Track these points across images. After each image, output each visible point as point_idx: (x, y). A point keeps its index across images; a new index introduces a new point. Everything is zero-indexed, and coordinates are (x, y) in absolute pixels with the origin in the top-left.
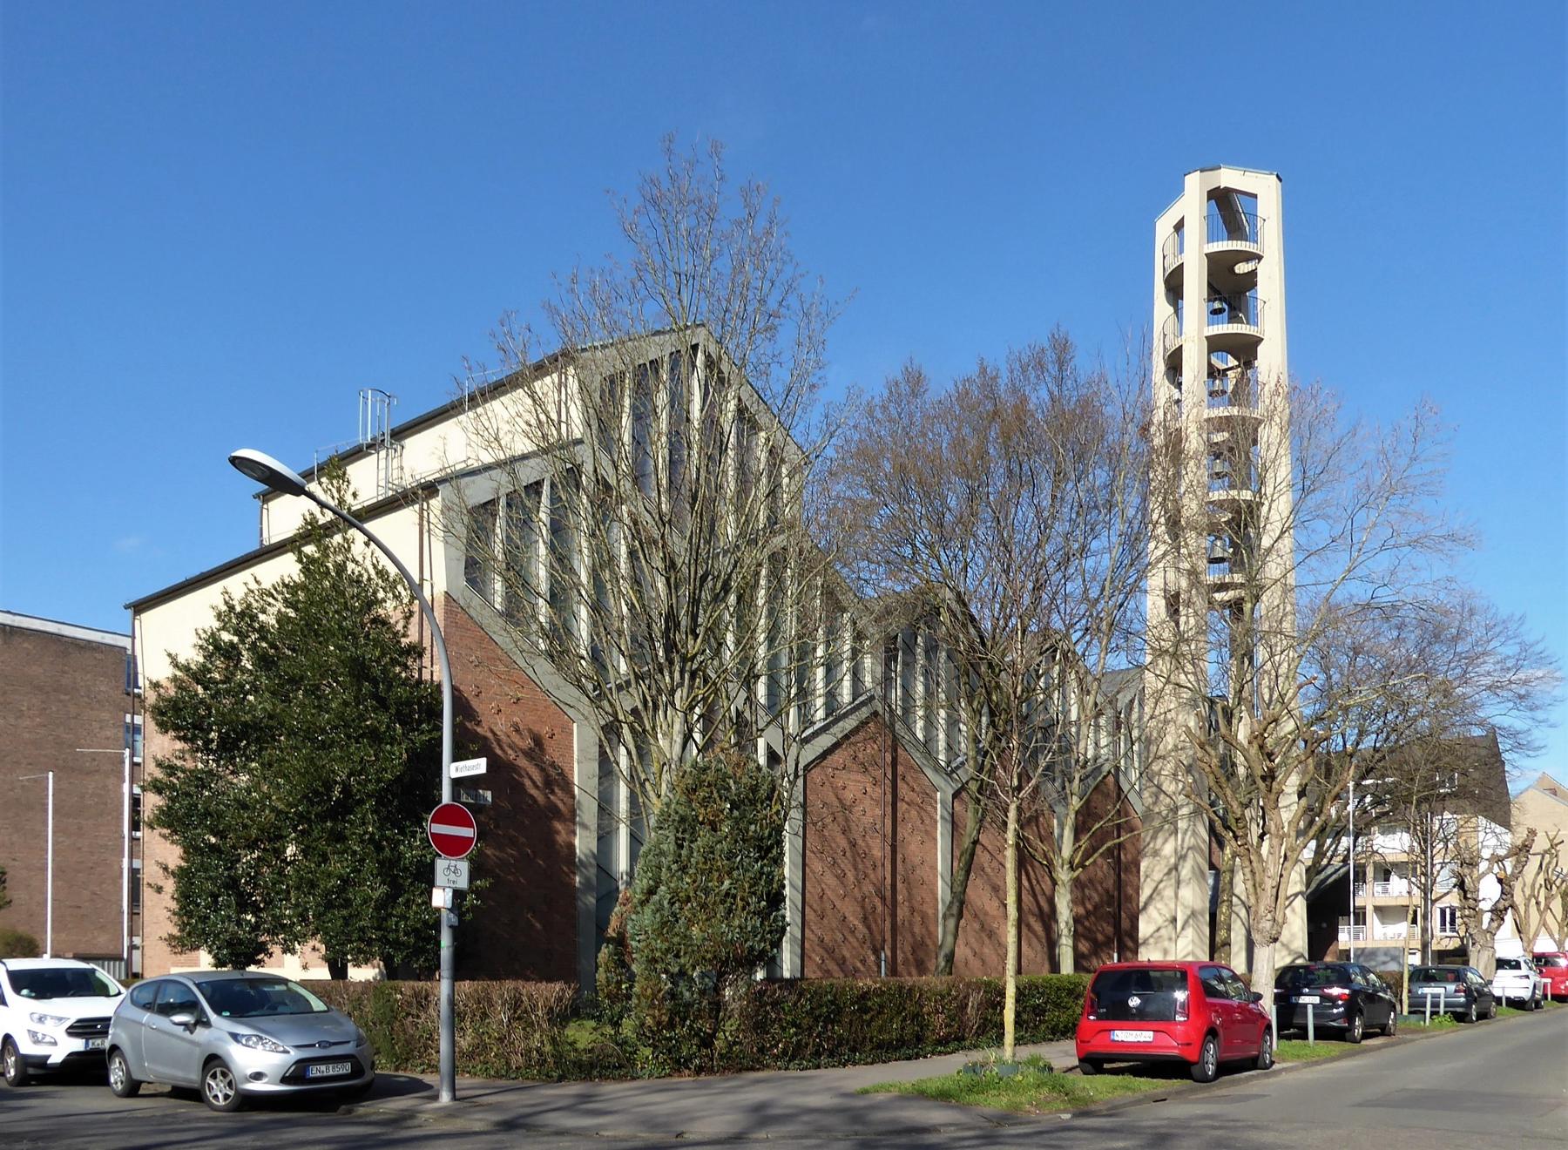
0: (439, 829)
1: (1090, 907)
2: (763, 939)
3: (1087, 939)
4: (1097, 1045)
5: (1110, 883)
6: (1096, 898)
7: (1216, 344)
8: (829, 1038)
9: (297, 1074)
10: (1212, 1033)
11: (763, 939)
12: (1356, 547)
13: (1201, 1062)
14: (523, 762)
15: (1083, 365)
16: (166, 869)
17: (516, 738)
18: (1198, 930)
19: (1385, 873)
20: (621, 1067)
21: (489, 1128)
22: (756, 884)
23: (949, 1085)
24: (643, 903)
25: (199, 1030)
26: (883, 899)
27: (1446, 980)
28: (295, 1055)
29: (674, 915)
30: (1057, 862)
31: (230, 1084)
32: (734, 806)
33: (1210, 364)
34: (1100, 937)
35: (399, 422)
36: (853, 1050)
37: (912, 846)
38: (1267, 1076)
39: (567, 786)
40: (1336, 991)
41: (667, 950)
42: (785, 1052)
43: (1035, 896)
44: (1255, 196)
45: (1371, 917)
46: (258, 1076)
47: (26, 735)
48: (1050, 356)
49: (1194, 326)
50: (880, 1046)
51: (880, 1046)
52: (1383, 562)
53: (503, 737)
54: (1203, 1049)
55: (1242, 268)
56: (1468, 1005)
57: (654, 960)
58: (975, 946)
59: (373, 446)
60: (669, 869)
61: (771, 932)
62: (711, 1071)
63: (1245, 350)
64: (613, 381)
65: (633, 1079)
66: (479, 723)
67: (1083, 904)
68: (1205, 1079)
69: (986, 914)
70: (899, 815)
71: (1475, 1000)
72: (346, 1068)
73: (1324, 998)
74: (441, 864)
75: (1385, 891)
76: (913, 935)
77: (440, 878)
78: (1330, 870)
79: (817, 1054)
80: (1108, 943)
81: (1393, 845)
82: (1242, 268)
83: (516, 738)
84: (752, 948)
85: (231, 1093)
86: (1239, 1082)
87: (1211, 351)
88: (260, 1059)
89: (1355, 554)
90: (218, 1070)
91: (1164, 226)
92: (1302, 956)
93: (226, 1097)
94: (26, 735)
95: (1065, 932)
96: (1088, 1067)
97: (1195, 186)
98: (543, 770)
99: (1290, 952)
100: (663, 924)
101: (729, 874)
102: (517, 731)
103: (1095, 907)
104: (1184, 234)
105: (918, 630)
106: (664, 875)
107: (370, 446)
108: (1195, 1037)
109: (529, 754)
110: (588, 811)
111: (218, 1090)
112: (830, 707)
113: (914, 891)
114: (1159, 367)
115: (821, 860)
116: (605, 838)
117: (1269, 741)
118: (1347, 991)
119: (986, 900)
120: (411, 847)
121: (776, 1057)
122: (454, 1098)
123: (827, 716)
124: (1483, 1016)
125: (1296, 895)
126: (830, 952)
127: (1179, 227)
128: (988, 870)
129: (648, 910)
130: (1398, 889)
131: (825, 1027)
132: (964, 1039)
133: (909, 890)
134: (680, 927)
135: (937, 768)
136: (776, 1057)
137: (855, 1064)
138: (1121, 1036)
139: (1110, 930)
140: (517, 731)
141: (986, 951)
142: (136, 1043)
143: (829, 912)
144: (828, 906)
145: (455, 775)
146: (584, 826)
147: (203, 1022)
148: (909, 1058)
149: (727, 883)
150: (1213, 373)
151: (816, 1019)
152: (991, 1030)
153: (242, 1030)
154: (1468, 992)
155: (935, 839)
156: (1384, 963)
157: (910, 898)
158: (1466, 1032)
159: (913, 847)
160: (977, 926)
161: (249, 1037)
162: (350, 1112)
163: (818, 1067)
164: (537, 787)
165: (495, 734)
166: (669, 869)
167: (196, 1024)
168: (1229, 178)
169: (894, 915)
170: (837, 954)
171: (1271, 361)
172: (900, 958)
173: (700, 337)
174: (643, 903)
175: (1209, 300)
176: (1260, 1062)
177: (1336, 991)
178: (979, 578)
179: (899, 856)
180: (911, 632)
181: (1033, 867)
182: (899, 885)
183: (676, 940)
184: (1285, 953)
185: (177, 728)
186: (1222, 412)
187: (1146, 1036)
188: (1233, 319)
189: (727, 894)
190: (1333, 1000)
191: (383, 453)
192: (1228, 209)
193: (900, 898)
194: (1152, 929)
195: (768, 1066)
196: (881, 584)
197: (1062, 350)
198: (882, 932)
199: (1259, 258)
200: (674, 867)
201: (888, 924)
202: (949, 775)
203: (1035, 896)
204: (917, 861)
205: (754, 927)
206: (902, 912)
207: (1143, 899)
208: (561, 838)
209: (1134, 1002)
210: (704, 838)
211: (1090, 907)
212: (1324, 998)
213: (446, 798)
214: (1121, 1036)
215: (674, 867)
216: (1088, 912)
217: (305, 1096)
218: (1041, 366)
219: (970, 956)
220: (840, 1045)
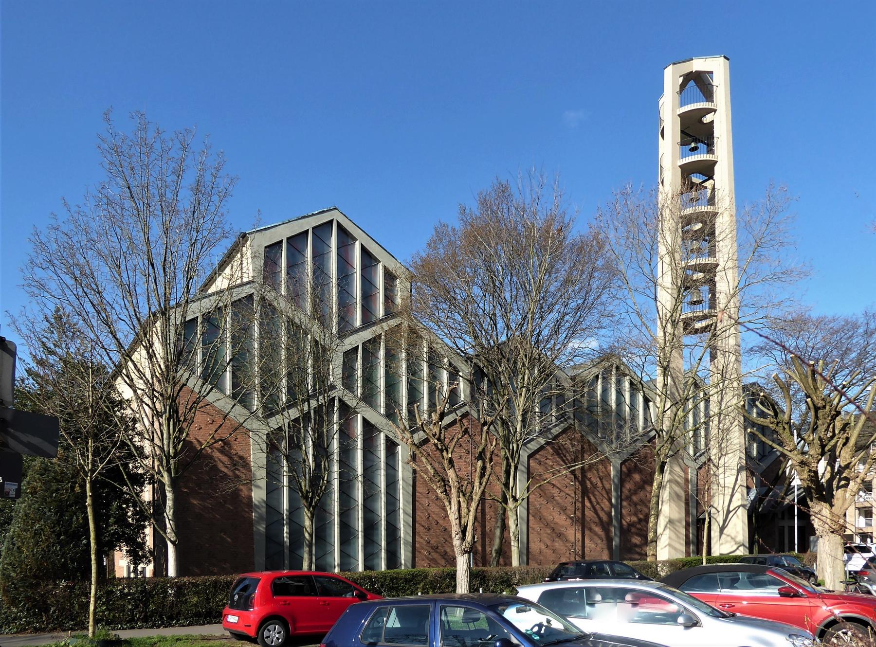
1: (641, 516)
7: (687, 171)
14: (216, 454)
18: (676, 531)
39: (246, 465)
43: (596, 511)
50: (198, 615)
51: (198, 615)
58: (549, 543)
63: (707, 170)
64: (273, 248)
82: (707, 119)
97: (671, 77)
98: (230, 458)
109: (222, 451)
110: (260, 475)
115: (428, 498)
116: (273, 490)
119: (556, 515)
125: (739, 507)
126: (435, 549)
128: (557, 498)
141: (557, 545)
144: (434, 523)
146: (258, 487)
163: (133, 628)
164: (227, 467)
168: (698, 65)
173: (336, 216)
181: (594, 495)
182: (487, 510)
192: (700, 83)
193: (488, 517)
197: (504, 192)
199: (715, 111)
203: (596, 511)
208: (244, 492)
219: (543, 547)
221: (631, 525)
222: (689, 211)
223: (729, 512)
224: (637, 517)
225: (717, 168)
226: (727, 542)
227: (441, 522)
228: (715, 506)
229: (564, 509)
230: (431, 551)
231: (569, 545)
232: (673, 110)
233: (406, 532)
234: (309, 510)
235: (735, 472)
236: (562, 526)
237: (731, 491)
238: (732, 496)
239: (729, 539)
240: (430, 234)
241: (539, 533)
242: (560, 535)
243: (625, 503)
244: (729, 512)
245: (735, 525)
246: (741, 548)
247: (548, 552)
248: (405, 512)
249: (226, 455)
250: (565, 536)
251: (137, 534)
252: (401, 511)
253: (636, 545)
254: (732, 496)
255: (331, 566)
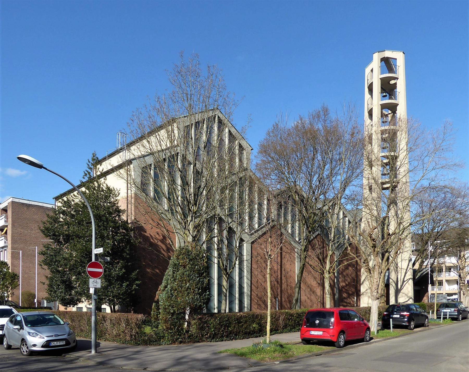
0: (90, 269)
1: (347, 283)
2: (200, 302)
3: (346, 293)
4: (306, 336)
5: (353, 275)
6: (349, 280)
7: (383, 107)
8: (226, 332)
9: (47, 344)
10: (342, 332)
11: (200, 302)
12: (425, 169)
13: (338, 341)
14: (160, 243)
15: (332, 116)
16: (47, 277)
17: (157, 236)
19: (449, 269)
20: (156, 341)
21: (95, 364)
22: (197, 285)
23: (244, 351)
24: (163, 290)
25: (21, 331)
26: (278, 282)
27: (451, 307)
28: (46, 339)
29: (172, 294)
30: (325, 271)
31: (27, 348)
32: (191, 260)
33: (382, 112)
34: (350, 292)
35: (129, 141)
36: (236, 335)
37: (287, 266)
38: (366, 344)
40: (405, 313)
41: (170, 305)
42: (210, 336)
44: (396, 59)
45: (445, 283)
46: (35, 345)
47: (34, 236)
48: (322, 113)
49: (375, 101)
50: (246, 333)
51: (246, 333)
52: (433, 174)
53: (153, 236)
54: (338, 337)
55: (392, 82)
56: (458, 315)
57: (166, 309)
58: (309, 296)
59: (122, 149)
60: (170, 280)
61: (203, 299)
62: (185, 343)
63: (393, 108)
64: (188, 128)
65: (160, 345)
66: (145, 232)
67: (345, 282)
68: (340, 347)
69: (312, 286)
70: (283, 256)
71: (461, 313)
72: (63, 343)
73: (401, 315)
74: (91, 280)
75: (449, 275)
76: (288, 293)
77: (91, 285)
78: (424, 270)
79: (222, 337)
80: (353, 294)
81: (451, 261)
82: (392, 82)
83: (157, 236)
84: (196, 305)
85: (28, 350)
86: (354, 347)
87: (382, 109)
88: (37, 340)
89: (424, 172)
90: (24, 343)
91: (368, 70)
92: (411, 298)
93: (26, 351)
94: (34, 236)
95: (327, 293)
96: (304, 342)
97: (377, 57)
98: (166, 246)
99: (408, 297)
100: (169, 297)
101: (189, 281)
102: (158, 234)
103: (349, 283)
104: (374, 73)
105: (288, 199)
106: (169, 282)
107: (121, 149)
108: (336, 334)
111: (24, 349)
112: (260, 224)
113: (288, 280)
114: (366, 114)
115: (257, 271)
117: (373, 236)
118: (408, 313)
120: (115, 271)
121: (207, 338)
122: (96, 352)
123: (259, 227)
124: (464, 318)
125: (410, 279)
126: (260, 298)
127: (372, 71)
129: (164, 293)
130: (454, 275)
131: (225, 329)
132: (278, 330)
133: (287, 278)
134: (173, 298)
135: (295, 241)
136: (207, 338)
137: (236, 339)
138: (313, 333)
139: (353, 290)
140: (158, 234)
142: (8, 333)
143: (260, 286)
145: (96, 253)
147: (22, 328)
148: (257, 337)
149: (188, 284)
150: (382, 115)
151: (221, 326)
152: (261, 332)
153: (32, 331)
154: (459, 311)
155: (295, 263)
156: (442, 299)
157: (287, 281)
158: (456, 324)
159: (287, 266)
160: (309, 290)
161: (33, 333)
162: (65, 356)
163: (222, 341)
165: (151, 235)
166: (170, 280)
167: (20, 329)
168: (388, 54)
169: (281, 287)
170: (263, 299)
171: (401, 111)
172: (283, 299)
173: (217, 113)
174: (163, 290)
175: (381, 93)
176: (365, 340)
177: (405, 313)
178: (302, 184)
179: (283, 269)
180: (288, 199)
182: (283, 278)
183: (172, 302)
184: (406, 297)
185: (50, 236)
186: (387, 128)
187: (320, 333)
188: (390, 98)
189: (188, 288)
190: (404, 316)
191: (124, 152)
192: (388, 64)
193: (283, 282)
194: (364, 290)
195: (204, 341)
196: (273, 185)
197: (326, 111)
198: (277, 292)
199: (397, 79)
200: (172, 279)
201: (279, 290)
202: (299, 243)
204: (289, 270)
205: (197, 298)
206: (284, 286)
207: (362, 281)
209: (317, 322)
210: (181, 270)
211: (347, 283)
212: (401, 315)
213: (93, 260)
214: (313, 333)
215: (172, 279)
216: (347, 285)
217: (50, 351)
218: (319, 117)
219: (306, 298)
220: (230, 333)
221: (343, 287)
222: (383, 128)
223: (404, 281)
224: (345, 283)
225: (398, 108)
226: (402, 296)
227: (263, 284)
228: (392, 278)
229: (315, 278)
230: (259, 300)
231: (317, 297)
232: (378, 76)
233: (248, 290)
234: (226, 276)
235: (408, 261)
236: (315, 287)
237: (405, 271)
238: (406, 273)
239: (404, 295)
240: (270, 127)
241: (305, 291)
242: (314, 292)
243: (340, 276)
244: (404, 281)
245: (407, 288)
246: (411, 300)
247: (308, 301)
248: (247, 278)
249: (164, 244)
250: (316, 293)
251: (104, 288)
252: (245, 278)
253: (345, 298)
254: (406, 273)
255: (212, 308)
